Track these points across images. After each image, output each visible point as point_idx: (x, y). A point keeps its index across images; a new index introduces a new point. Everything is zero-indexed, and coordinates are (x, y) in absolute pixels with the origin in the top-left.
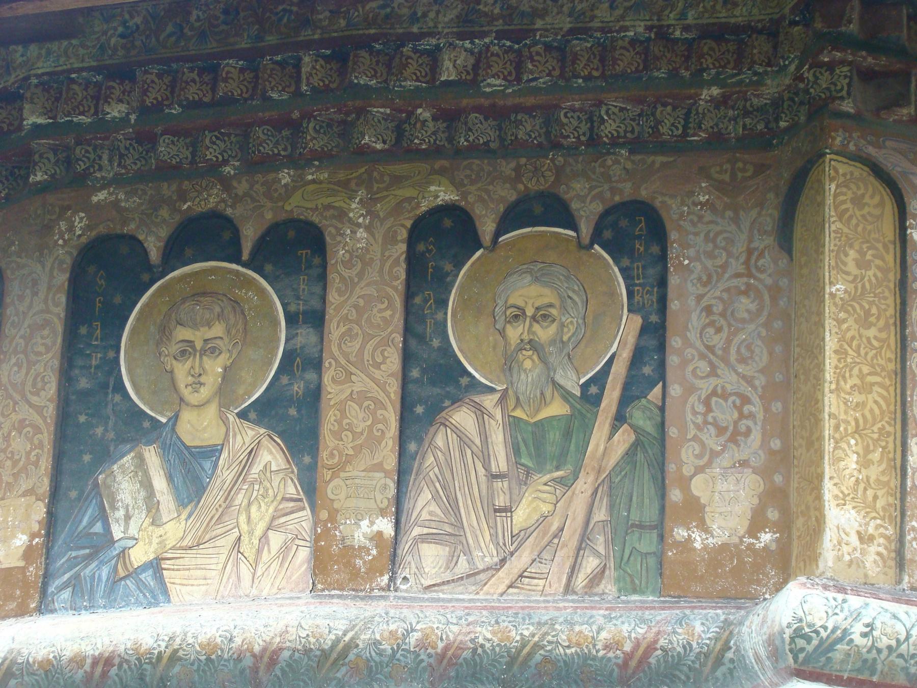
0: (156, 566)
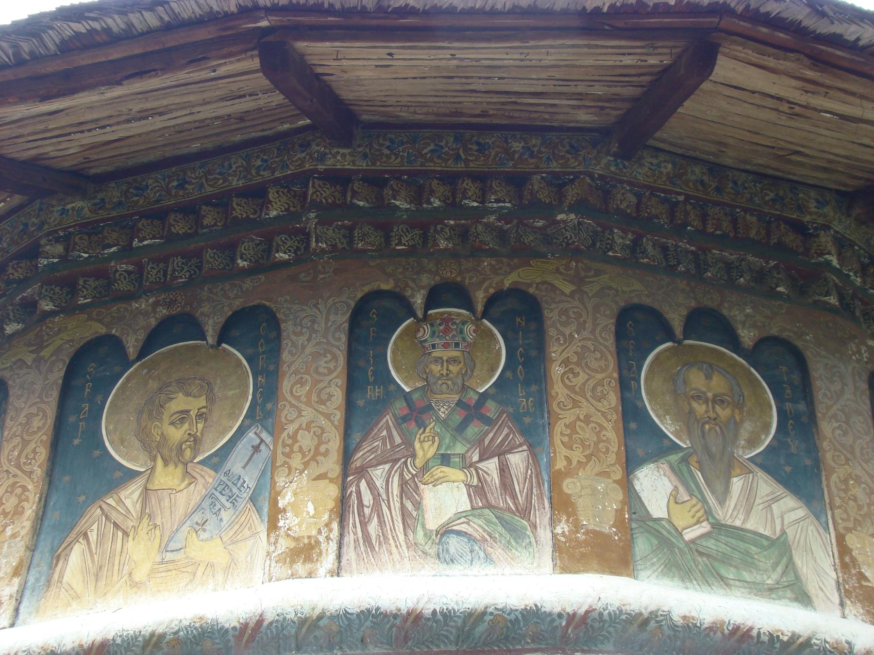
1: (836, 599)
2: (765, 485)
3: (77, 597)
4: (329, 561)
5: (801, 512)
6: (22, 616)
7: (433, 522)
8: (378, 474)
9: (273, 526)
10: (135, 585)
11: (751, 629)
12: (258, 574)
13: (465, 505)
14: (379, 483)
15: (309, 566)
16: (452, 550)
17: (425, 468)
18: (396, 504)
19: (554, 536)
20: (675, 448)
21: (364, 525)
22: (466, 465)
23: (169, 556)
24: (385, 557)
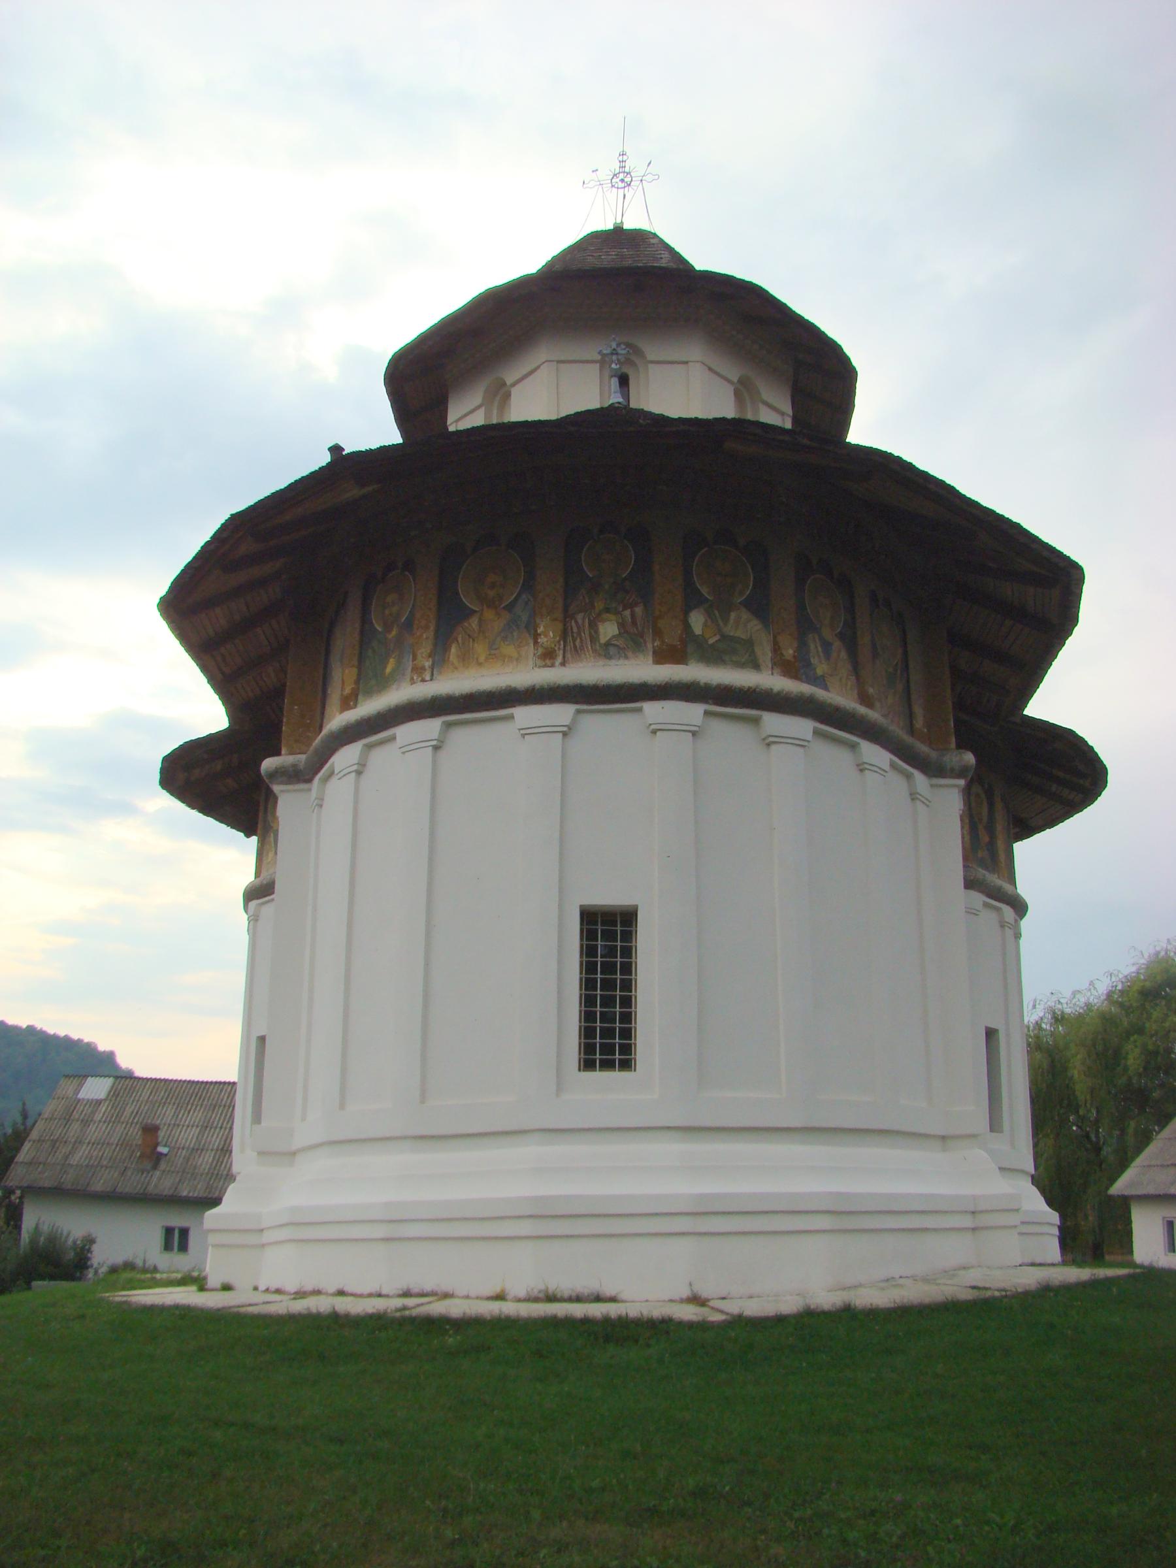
0: (823, 676)
1: (770, 665)
2: (745, 615)
3: (456, 668)
4: (559, 659)
5: (760, 626)
6: (435, 676)
7: (603, 640)
8: (580, 617)
9: (536, 643)
10: (480, 664)
11: (732, 686)
12: (531, 663)
13: (616, 632)
14: (580, 621)
15: (551, 661)
16: (611, 653)
17: (599, 614)
18: (587, 632)
19: (653, 647)
20: (707, 600)
21: (574, 641)
22: (617, 613)
23: (493, 652)
24: (583, 655)
